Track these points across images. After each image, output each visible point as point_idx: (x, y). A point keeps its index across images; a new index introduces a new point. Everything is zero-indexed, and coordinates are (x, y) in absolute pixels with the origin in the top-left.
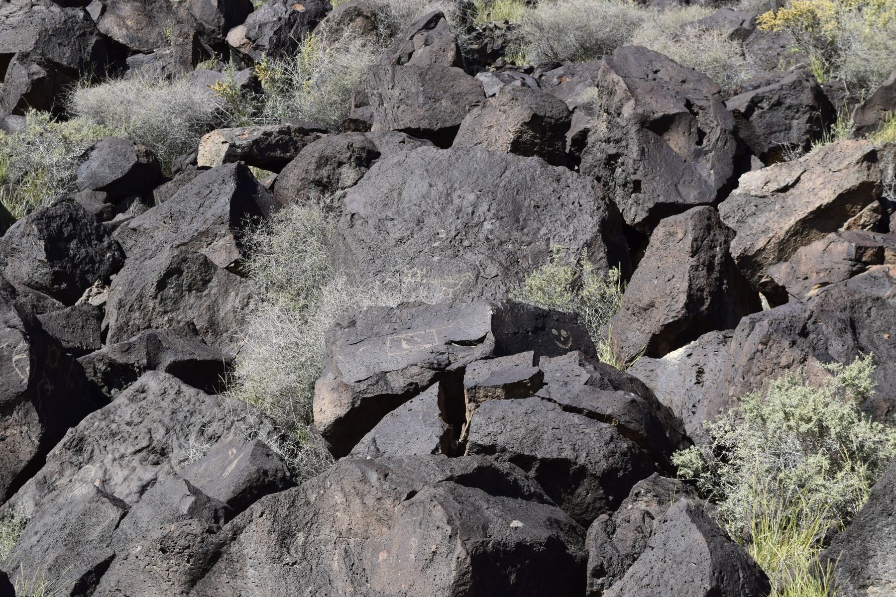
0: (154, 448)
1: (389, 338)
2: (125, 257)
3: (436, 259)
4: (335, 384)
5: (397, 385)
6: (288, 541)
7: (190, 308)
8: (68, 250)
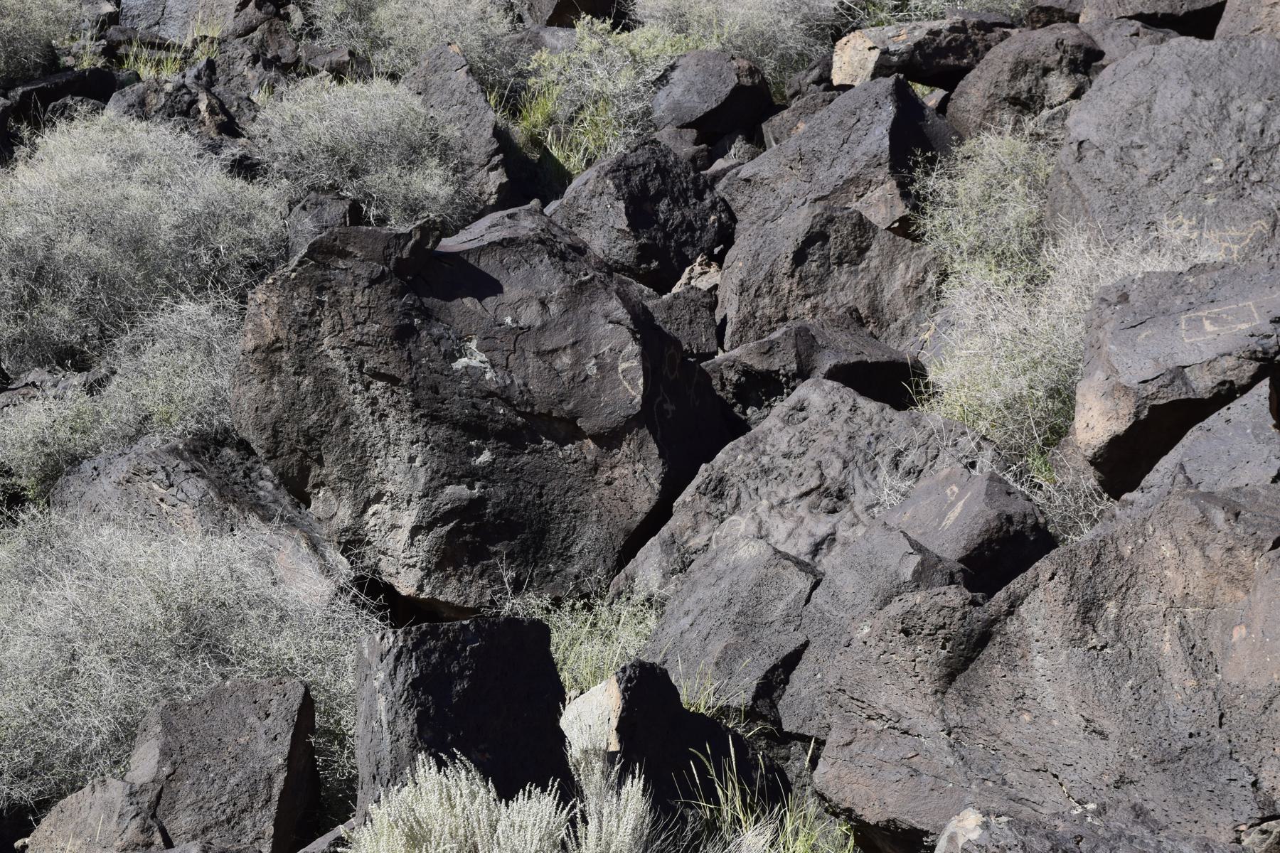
0: (827, 489)
1: (1183, 317)
2: (735, 221)
3: (1210, 202)
4: (1107, 387)
5: (1201, 385)
6: (1093, 614)
7: (842, 290)
8: (656, 213)
